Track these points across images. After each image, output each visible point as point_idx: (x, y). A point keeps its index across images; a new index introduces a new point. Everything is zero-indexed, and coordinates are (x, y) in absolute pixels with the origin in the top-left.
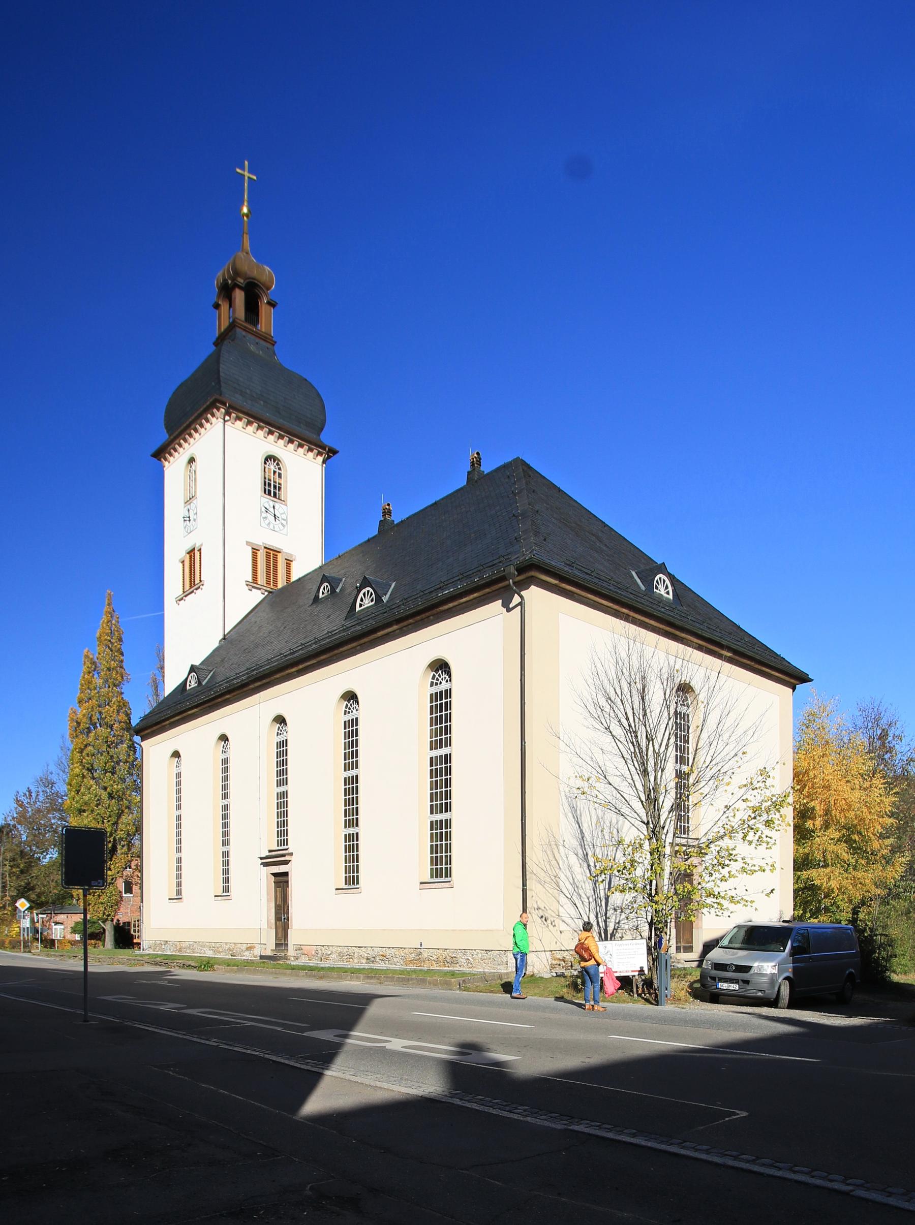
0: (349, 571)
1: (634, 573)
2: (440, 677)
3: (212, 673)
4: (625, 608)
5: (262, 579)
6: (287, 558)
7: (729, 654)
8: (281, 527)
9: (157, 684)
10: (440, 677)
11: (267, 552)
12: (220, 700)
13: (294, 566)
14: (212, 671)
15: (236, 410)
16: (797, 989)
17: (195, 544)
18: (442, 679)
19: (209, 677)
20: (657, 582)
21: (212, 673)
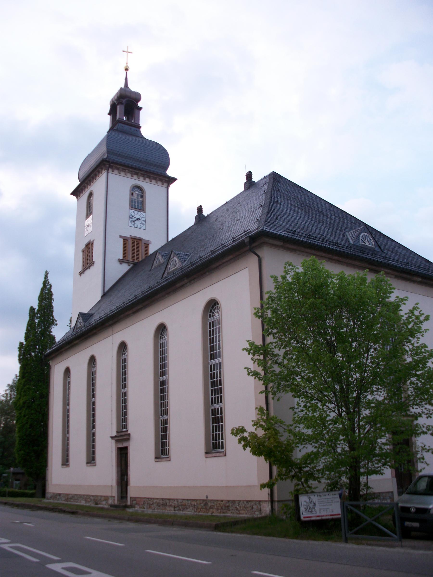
2: (215, 311)
5: (130, 258)
6: (145, 243)
7: (420, 279)
8: (142, 225)
10: (215, 311)
11: (132, 241)
16: (351, 241)
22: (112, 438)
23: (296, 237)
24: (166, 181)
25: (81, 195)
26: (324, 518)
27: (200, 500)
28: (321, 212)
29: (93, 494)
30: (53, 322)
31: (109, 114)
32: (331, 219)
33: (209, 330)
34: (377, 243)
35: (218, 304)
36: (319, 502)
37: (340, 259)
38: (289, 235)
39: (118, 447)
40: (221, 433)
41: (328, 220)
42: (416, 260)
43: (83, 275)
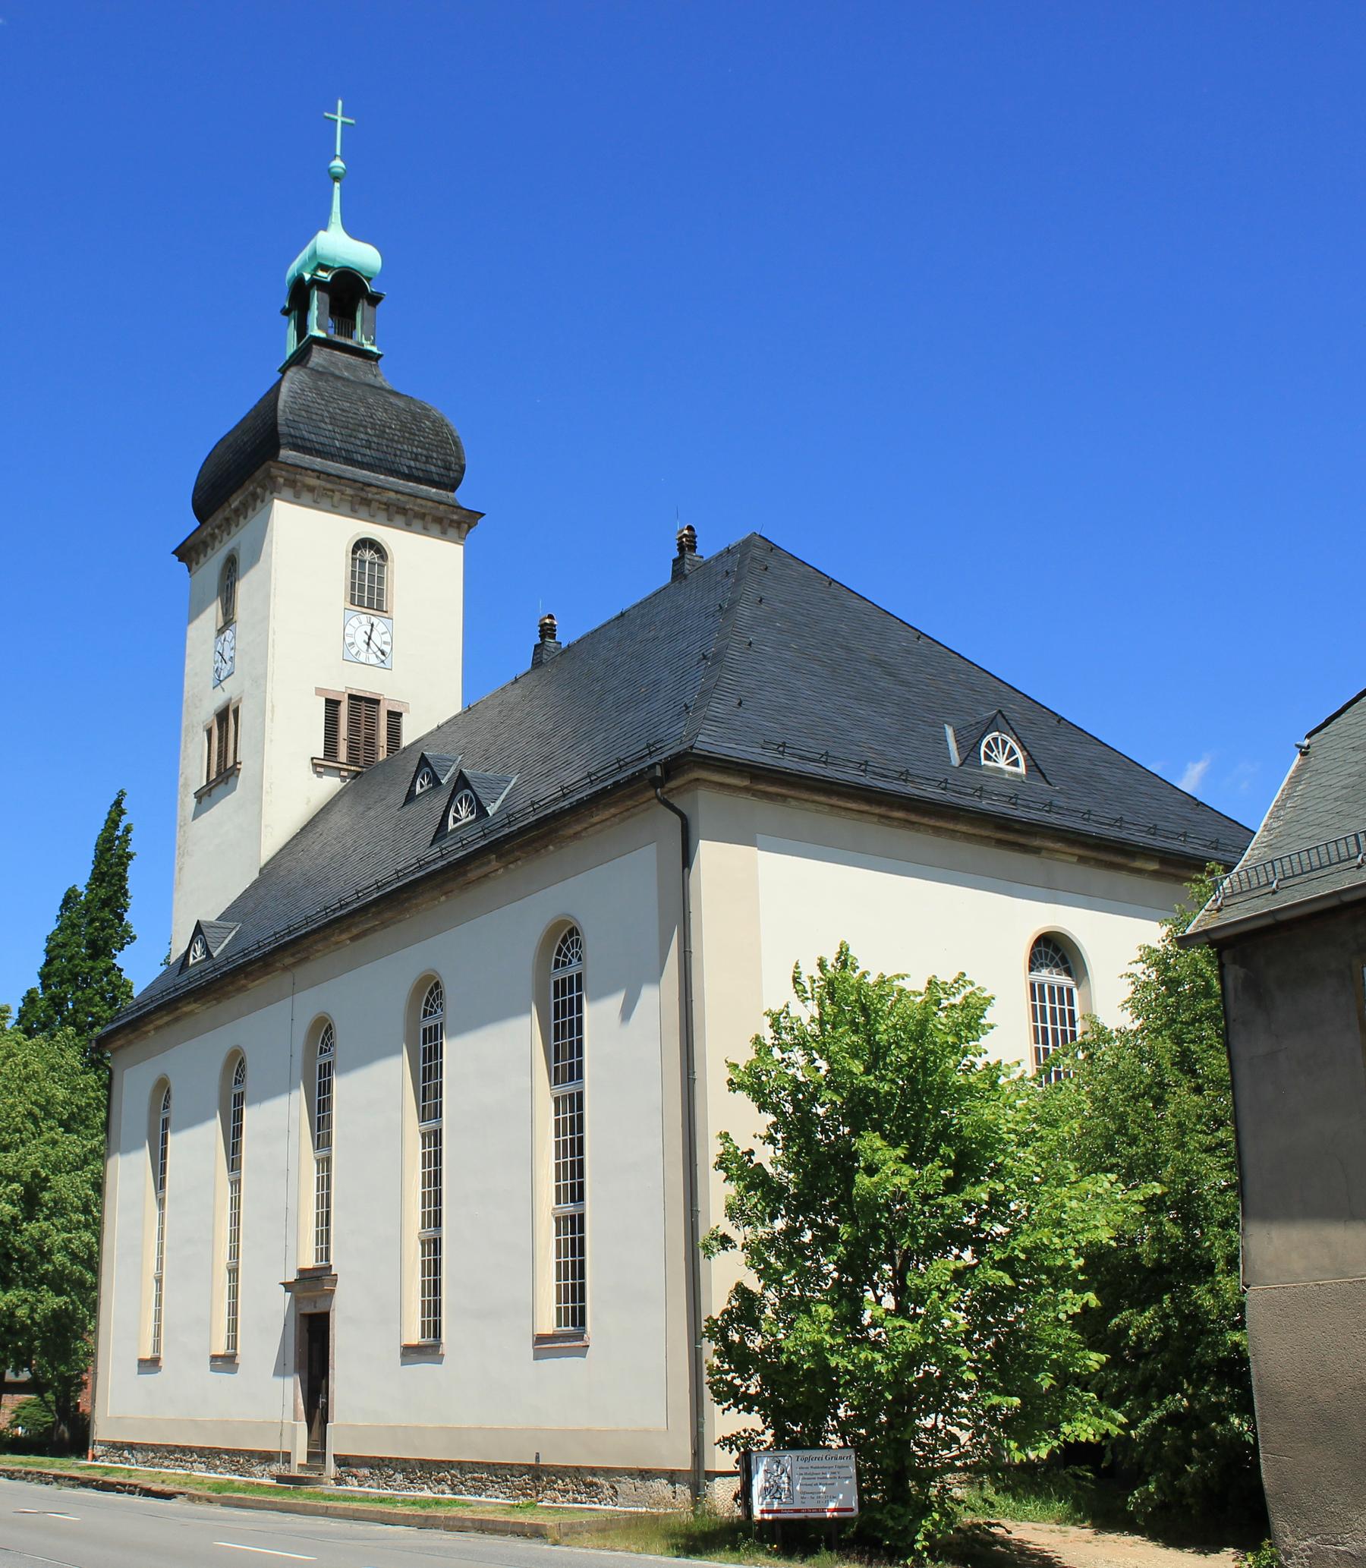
1: (949, 731)
2: (569, 952)
3: (234, 933)
7: (1154, 866)
10: (569, 952)
12: (712, 762)
13: (406, 722)
17: (231, 699)
18: (572, 955)
19: (226, 941)
20: (988, 746)
21: (234, 933)
22: (288, 1286)
24: (457, 525)
26: (811, 1515)
27: (520, 1465)
33: (553, 1001)
34: (1033, 760)
37: (913, 818)
39: (302, 1312)
40: (579, 1283)
43: (205, 799)
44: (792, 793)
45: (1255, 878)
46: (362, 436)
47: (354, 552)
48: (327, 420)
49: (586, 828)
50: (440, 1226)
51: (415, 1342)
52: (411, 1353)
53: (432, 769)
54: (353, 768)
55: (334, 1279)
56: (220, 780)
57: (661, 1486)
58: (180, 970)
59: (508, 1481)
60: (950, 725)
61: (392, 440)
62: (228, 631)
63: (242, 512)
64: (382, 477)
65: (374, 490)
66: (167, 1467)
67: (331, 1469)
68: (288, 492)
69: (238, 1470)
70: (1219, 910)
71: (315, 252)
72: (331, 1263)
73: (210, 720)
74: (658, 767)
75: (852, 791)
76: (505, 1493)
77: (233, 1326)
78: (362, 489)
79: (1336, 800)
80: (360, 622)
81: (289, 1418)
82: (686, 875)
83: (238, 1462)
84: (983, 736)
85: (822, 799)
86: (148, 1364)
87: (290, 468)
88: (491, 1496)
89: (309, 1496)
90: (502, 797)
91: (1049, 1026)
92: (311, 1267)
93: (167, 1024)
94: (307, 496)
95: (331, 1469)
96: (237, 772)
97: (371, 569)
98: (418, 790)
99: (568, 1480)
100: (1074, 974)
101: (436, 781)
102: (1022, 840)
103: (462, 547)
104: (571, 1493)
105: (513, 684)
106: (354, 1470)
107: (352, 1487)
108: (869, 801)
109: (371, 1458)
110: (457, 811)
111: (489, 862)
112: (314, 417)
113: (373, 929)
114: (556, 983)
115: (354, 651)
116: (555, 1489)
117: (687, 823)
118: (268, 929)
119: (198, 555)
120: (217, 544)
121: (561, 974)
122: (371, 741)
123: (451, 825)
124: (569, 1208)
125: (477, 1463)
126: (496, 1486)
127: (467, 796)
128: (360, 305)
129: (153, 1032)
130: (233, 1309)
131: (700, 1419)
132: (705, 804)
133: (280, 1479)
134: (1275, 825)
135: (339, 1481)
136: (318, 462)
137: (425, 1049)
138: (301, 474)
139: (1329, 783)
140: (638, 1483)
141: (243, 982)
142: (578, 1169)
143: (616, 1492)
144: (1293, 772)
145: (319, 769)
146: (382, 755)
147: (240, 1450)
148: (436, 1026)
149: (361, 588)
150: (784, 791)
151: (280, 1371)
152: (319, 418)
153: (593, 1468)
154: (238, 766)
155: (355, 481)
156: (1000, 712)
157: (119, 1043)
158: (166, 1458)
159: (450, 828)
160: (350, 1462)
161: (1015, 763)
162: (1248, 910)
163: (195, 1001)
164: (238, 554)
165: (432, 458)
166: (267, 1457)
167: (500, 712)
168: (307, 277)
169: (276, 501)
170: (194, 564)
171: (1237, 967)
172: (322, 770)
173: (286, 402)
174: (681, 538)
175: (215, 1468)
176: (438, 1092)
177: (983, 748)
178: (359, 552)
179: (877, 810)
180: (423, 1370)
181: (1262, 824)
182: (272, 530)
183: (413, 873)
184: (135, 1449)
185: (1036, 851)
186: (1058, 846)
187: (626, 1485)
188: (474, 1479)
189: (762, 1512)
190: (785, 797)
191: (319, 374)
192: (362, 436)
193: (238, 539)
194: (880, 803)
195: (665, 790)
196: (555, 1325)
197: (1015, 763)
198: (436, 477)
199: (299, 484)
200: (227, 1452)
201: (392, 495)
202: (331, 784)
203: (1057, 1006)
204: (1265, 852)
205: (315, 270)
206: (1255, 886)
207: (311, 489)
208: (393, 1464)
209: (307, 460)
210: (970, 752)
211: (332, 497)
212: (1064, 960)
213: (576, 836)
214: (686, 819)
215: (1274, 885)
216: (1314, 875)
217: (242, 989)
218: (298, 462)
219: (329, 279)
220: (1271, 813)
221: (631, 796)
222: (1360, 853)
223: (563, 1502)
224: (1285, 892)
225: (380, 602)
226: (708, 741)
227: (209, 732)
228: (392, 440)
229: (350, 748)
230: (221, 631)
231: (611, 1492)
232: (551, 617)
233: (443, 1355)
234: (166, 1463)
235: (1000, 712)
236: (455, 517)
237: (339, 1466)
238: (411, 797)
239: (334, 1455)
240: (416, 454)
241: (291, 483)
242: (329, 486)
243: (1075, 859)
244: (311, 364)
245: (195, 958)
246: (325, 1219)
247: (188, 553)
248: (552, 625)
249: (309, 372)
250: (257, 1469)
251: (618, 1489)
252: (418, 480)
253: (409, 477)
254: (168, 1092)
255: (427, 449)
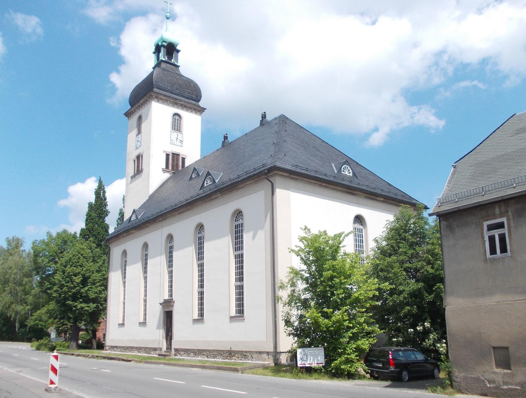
0: (206, 165)
1: (333, 165)
3: (143, 212)
4: (324, 183)
7: (382, 199)
9: (149, 194)
14: (144, 211)
15: (159, 98)
17: (140, 153)
19: (142, 214)
20: (344, 168)
21: (143, 212)
22: (161, 304)
23: (298, 170)
24: (199, 111)
25: (132, 116)
27: (226, 350)
28: (315, 147)
29: (144, 346)
30: (106, 213)
31: (154, 53)
32: (322, 153)
35: (242, 213)
36: (310, 354)
37: (328, 185)
38: (293, 169)
41: (320, 154)
42: (381, 184)
43: (134, 179)
44: (299, 178)
45: (448, 198)
46: (175, 86)
47: (173, 116)
48: (166, 82)
49: (244, 186)
50: (203, 287)
51: (196, 318)
52: (195, 321)
53: (197, 171)
54: (173, 171)
55: (174, 302)
56: (137, 173)
57: (265, 356)
58: (129, 222)
59: (222, 354)
60: (333, 163)
61: (183, 88)
62: (139, 135)
63: (143, 104)
64: (180, 97)
65: (179, 101)
66: (127, 352)
67: (173, 352)
68: (156, 100)
69: (147, 352)
70: (439, 206)
71: (162, 37)
72: (173, 297)
73: (135, 158)
74: (266, 170)
75: (313, 178)
76: (222, 358)
77: (145, 314)
78: (175, 100)
79: (468, 179)
80: (175, 134)
81: (161, 339)
82: (273, 197)
83: (147, 350)
84: (342, 166)
85: (306, 180)
86: (121, 325)
87: (156, 93)
88: (218, 359)
89: (169, 360)
90: (219, 178)
91: (357, 238)
92: (167, 299)
93: (126, 235)
94: (161, 101)
95: (173, 352)
96: (142, 172)
97: (178, 121)
98: (193, 176)
99: (239, 354)
100: (363, 225)
101: (198, 175)
102: (352, 192)
103: (201, 117)
104: (240, 358)
105: (216, 151)
106: (180, 352)
107: (179, 357)
108: (317, 180)
109: (184, 349)
110: (207, 181)
111: (218, 194)
112: (163, 81)
113: (185, 211)
114: (235, 225)
115: (173, 142)
116: (235, 357)
117: (273, 185)
118: (155, 210)
119: (131, 115)
120: (136, 113)
121: (237, 223)
122: (177, 165)
123: (205, 185)
124: (239, 283)
125: (214, 350)
126: (219, 356)
127: (210, 177)
128: (174, 53)
129: (122, 238)
130: (145, 310)
131: (276, 338)
132: (277, 180)
133: (159, 355)
134: (450, 185)
135: (175, 355)
136: (164, 92)
137: (199, 242)
138: (159, 95)
139: (464, 175)
140: (259, 355)
141: (148, 225)
142: (242, 273)
143: (252, 357)
144: (452, 172)
145: (164, 171)
146: (180, 168)
147: (147, 347)
148: (202, 236)
149: (175, 125)
150: (297, 177)
151: (158, 328)
152: (164, 81)
153: (246, 351)
154: (143, 170)
155: (173, 98)
156: (346, 160)
157: (112, 240)
158: (126, 350)
159: (205, 186)
160: (179, 350)
161: (350, 173)
162: (449, 207)
163: (134, 230)
164: (142, 115)
165: (193, 93)
166: (155, 349)
167: (214, 158)
168: (160, 44)
169: (153, 102)
170: (130, 118)
171: (444, 222)
172: (165, 172)
173: (155, 76)
174: (262, 115)
175: (140, 352)
176: (202, 253)
177: (342, 169)
178: (174, 116)
179: (319, 183)
180: (199, 326)
181: (446, 185)
182: (152, 109)
183: (196, 197)
184: (117, 348)
185: (355, 195)
186: (361, 194)
187: (255, 356)
188: (213, 354)
189: (300, 364)
190: (297, 179)
191: (164, 69)
192: (175, 86)
193: (142, 111)
194: (320, 181)
195: (267, 176)
196: (235, 314)
197: (350, 173)
198: (194, 99)
199: (159, 98)
200: (144, 348)
201: (183, 102)
202: (167, 175)
203: (359, 233)
204: (448, 192)
205: (162, 42)
206: (448, 201)
207: (162, 99)
208: (191, 350)
209: (161, 92)
210: (340, 170)
211: (167, 102)
212: (361, 222)
213: (242, 187)
214: (273, 184)
215: (456, 200)
216: (468, 198)
217: (147, 226)
218: (158, 92)
219: (166, 45)
220: (448, 182)
221: (257, 178)
222: (483, 192)
223: (238, 360)
224: (459, 202)
225: (180, 130)
226: (278, 164)
227: (134, 161)
228: (183, 88)
229: (172, 166)
230: (137, 135)
231: (251, 357)
232: (227, 134)
233: (204, 322)
234: (126, 351)
235: (346, 160)
236: (199, 109)
237: (175, 351)
238: (191, 178)
239: (174, 348)
240: (189, 92)
241: (157, 97)
242: (167, 99)
243: (364, 197)
244: (161, 67)
245: (133, 219)
246: (171, 286)
247: (128, 114)
248: (227, 136)
249: (161, 69)
250: (152, 352)
251: (253, 356)
252: (190, 99)
253: (187, 98)
254: (126, 253)
255: (192, 91)
